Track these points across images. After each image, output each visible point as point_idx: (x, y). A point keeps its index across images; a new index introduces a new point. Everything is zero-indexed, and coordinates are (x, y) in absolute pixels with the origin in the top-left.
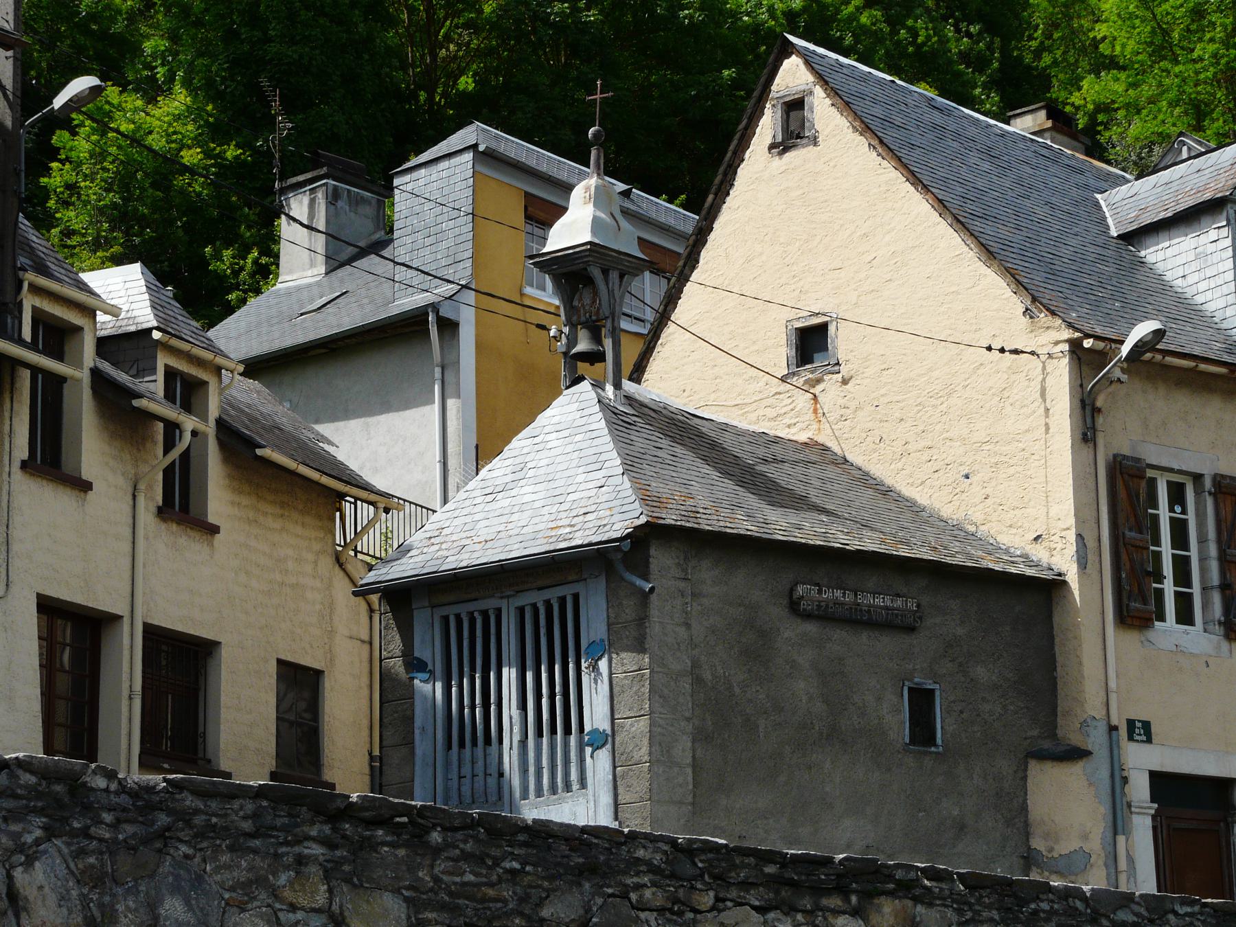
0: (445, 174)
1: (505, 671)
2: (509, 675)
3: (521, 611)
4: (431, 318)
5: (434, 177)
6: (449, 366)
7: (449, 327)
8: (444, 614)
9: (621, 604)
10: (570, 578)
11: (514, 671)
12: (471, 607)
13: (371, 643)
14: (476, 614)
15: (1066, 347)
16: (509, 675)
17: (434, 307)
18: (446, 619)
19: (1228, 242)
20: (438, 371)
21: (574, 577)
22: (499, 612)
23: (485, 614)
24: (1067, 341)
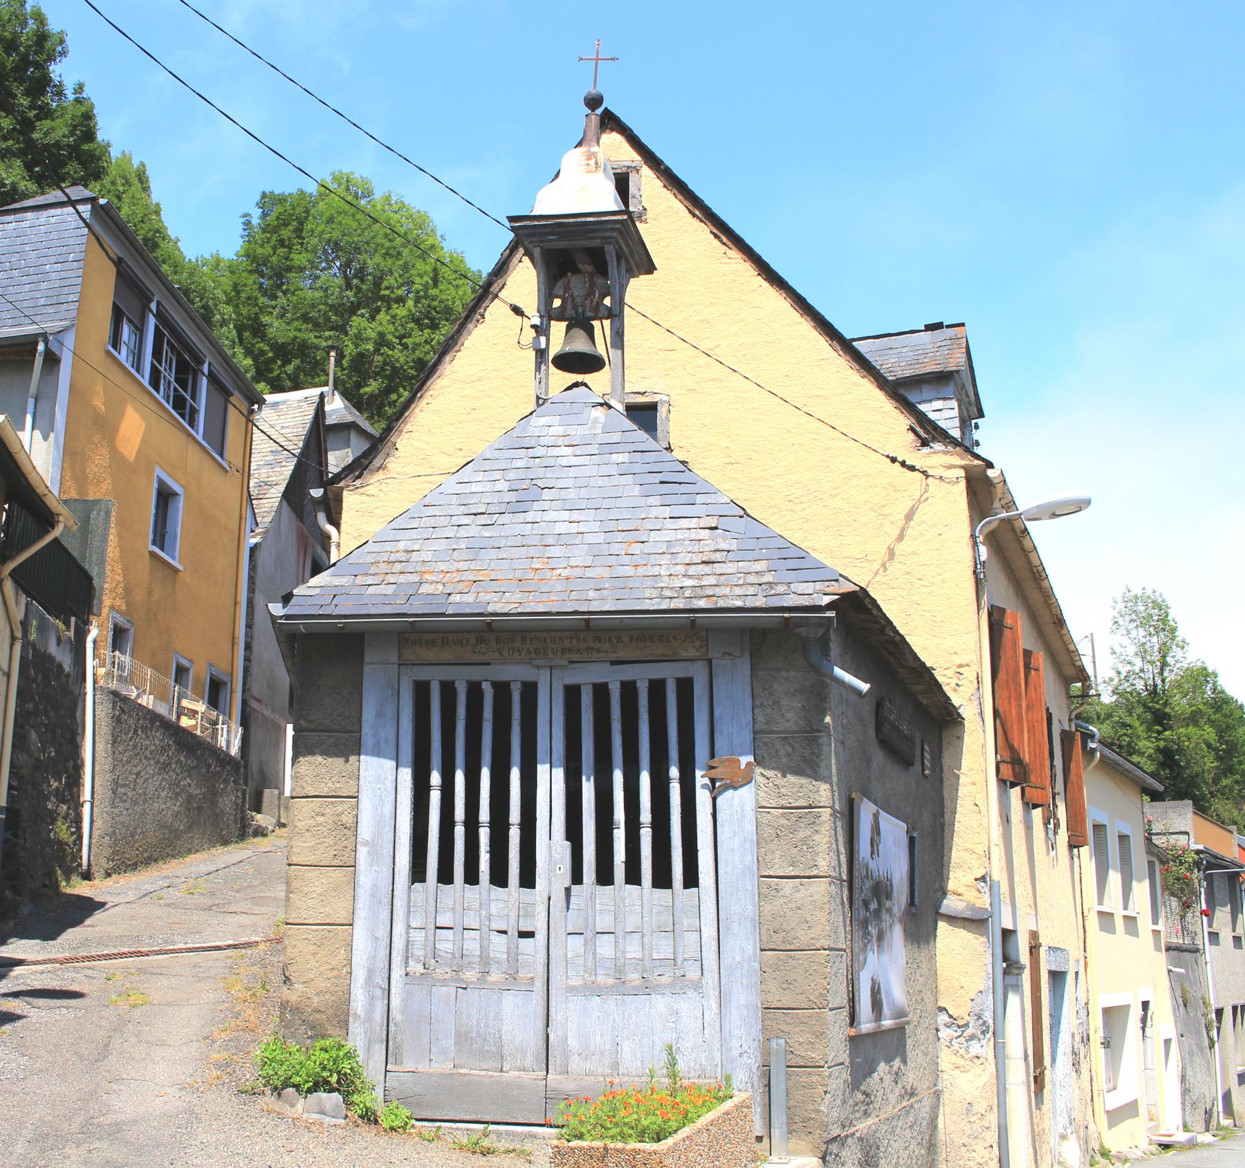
0: (53, 220)
1: (542, 770)
2: (551, 781)
3: (572, 694)
4: (41, 347)
5: (42, 220)
6: (45, 397)
7: (52, 360)
8: (422, 677)
9: (776, 703)
10: (684, 654)
11: (559, 774)
12: (475, 673)
13: (8, 675)
14: (486, 687)
15: (962, 473)
16: (551, 781)
17: (44, 336)
18: (422, 690)
19: (955, 413)
20: (31, 402)
21: (691, 653)
22: (530, 691)
23: (497, 685)
24: (962, 467)
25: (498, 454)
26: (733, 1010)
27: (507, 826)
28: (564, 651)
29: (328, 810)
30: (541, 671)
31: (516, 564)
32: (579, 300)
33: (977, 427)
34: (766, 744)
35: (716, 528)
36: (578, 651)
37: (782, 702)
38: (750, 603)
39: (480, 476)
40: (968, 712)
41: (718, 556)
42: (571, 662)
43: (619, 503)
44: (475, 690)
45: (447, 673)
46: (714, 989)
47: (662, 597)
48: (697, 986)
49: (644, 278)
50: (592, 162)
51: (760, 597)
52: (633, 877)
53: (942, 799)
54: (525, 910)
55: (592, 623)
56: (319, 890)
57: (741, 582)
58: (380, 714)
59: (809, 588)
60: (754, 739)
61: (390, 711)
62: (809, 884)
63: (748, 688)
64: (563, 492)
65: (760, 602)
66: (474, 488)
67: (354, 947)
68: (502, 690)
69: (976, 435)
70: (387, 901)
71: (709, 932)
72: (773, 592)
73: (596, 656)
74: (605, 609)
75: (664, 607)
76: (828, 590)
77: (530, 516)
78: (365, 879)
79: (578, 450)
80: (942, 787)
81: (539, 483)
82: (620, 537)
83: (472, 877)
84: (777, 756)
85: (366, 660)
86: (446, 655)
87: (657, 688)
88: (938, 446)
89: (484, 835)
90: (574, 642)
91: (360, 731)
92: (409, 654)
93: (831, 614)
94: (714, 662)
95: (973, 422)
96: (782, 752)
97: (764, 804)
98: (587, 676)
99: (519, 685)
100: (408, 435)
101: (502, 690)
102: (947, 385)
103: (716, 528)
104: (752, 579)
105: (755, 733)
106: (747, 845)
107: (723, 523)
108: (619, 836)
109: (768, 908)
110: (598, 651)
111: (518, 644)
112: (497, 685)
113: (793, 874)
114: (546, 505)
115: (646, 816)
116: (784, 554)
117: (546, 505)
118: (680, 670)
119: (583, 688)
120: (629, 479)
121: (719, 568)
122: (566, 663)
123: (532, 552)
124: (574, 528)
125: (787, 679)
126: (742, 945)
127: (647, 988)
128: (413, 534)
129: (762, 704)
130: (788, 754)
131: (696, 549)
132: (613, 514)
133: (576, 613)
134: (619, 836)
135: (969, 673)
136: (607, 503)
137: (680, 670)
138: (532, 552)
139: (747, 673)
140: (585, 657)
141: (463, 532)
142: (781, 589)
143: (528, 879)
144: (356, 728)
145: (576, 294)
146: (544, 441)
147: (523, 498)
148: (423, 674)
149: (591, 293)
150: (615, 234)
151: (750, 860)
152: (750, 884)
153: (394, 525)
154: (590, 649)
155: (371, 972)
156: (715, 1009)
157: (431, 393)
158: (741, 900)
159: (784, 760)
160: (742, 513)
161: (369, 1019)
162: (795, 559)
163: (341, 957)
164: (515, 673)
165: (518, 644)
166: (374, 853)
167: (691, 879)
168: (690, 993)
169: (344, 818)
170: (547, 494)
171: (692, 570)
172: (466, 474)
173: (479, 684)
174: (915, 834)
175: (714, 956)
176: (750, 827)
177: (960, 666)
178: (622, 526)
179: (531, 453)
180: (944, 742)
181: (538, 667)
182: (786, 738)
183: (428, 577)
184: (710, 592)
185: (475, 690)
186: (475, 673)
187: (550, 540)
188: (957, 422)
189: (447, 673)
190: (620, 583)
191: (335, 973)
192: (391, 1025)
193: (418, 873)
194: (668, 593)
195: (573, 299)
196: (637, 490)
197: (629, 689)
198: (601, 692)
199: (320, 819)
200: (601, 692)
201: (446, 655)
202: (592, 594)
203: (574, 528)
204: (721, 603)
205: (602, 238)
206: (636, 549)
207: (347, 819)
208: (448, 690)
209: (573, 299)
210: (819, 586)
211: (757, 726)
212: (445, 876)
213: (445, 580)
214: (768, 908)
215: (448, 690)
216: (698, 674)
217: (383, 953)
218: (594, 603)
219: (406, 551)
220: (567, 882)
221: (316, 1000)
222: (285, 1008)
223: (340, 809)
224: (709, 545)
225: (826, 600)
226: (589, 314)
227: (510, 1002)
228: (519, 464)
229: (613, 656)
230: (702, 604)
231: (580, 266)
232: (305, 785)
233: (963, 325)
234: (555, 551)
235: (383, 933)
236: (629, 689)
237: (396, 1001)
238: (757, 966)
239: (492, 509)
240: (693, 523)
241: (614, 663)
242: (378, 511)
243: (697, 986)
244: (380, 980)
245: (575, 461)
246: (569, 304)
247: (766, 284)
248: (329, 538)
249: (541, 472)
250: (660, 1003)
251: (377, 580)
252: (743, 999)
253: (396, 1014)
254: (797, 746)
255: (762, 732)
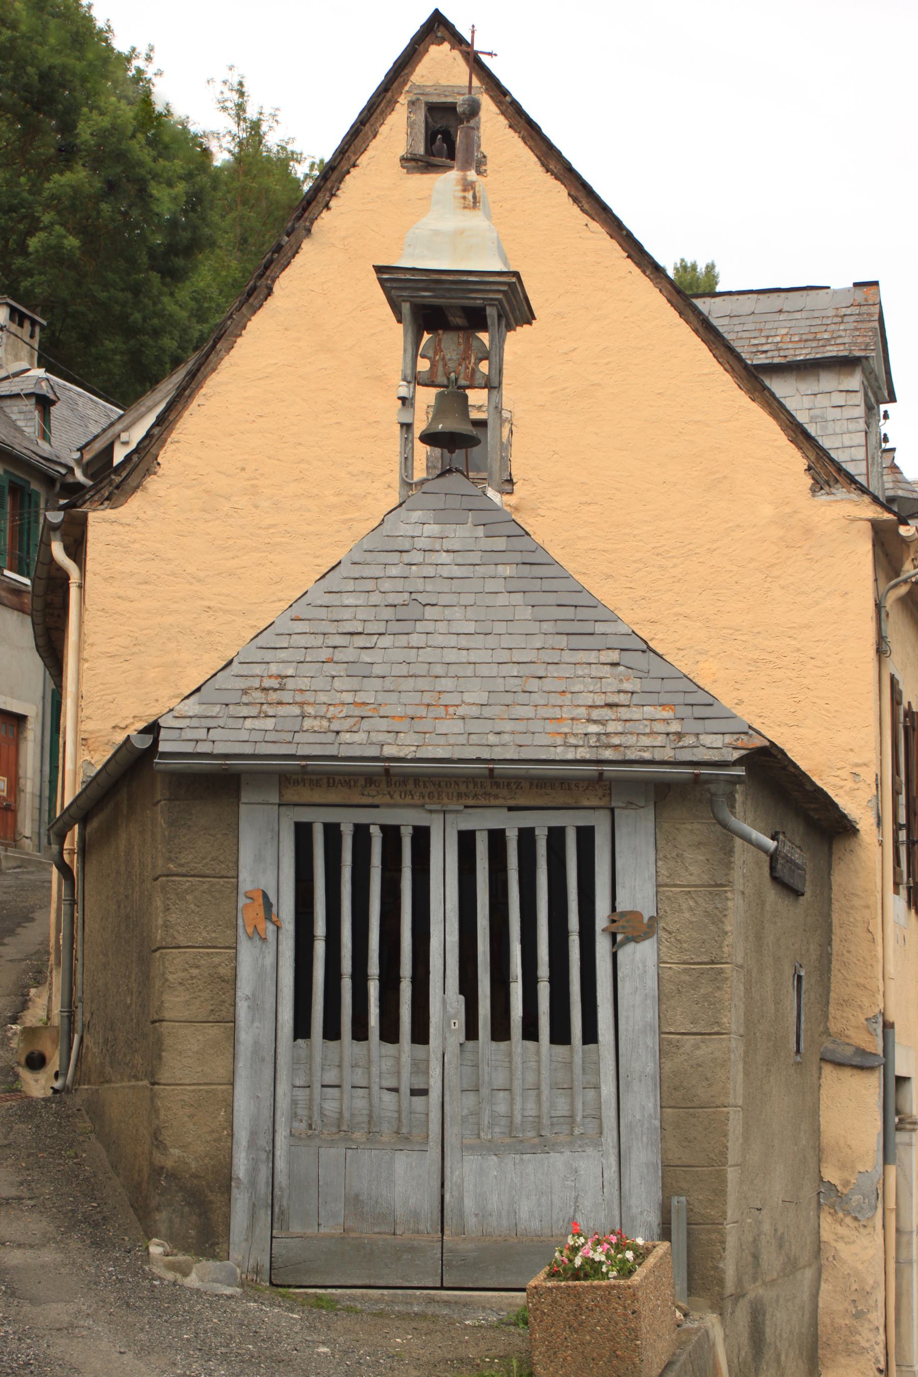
3: (466, 841)
10: (586, 803)
12: (362, 816)
14: (375, 831)
18: (303, 833)
21: (595, 802)
22: (422, 836)
24: (869, 520)
25: (369, 557)
26: (633, 1168)
27: (397, 980)
28: (460, 796)
29: (203, 962)
30: (434, 816)
31: (405, 698)
32: (451, 365)
33: (886, 416)
34: (668, 898)
35: (618, 664)
36: (475, 796)
37: (686, 854)
38: (659, 755)
39: (350, 585)
40: (865, 821)
41: (623, 699)
42: (466, 807)
43: (512, 627)
44: (361, 833)
45: (332, 816)
46: (613, 1147)
47: (566, 745)
48: (597, 1144)
49: (523, 331)
50: (469, 195)
51: (668, 749)
52: (530, 1032)
53: (830, 924)
54: (421, 1067)
55: (496, 772)
56: (195, 1048)
57: (648, 731)
58: (259, 858)
59: (718, 741)
60: (657, 892)
61: (270, 855)
62: (710, 1040)
63: (652, 840)
64: (447, 611)
65: (667, 754)
66: (349, 600)
67: (236, 1108)
68: (391, 834)
69: (885, 427)
70: (270, 1059)
71: (608, 1089)
72: (681, 744)
73: (493, 802)
74: (508, 757)
75: (570, 756)
76: (739, 743)
77: (415, 640)
78: (245, 1037)
79: (460, 559)
80: (830, 909)
81: (421, 598)
82: (515, 670)
83: (360, 1032)
84: (681, 911)
85: (243, 800)
86: (332, 797)
87: (556, 836)
88: (841, 493)
89: (374, 988)
90: (471, 786)
91: (237, 877)
92: (291, 795)
93: (740, 771)
94: (617, 812)
95: (883, 407)
96: (684, 906)
97: (666, 959)
98: (482, 822)
99: (410, 830)
100: (173, 447)
101: (391, 834)
102: (852, 373)
103: (618, 664)
104: (660, 727)
105: (658, 886)
106: (649, 1002)
107: (628, 658)
108: (517, 990)
109: (668, 1065)
110: (496, 797)
111: (411, 786)
112: (383, 828)
113: (694, 1030)
114: (430, 626)
115: (543, 971)
116: (690, 699)
117: (430, 626)
118: (583, 819)
119: (478, 834)
120: (518, 598)
121: (624, 713)
122: (462, 808)
123: (422, 684)
124: (463, 656)
125: (691, 831)
126: (642, 1103)
127: (545, 1146)
128: (282, 655)
129: (665, 857)
130: (691, 909)
131: (597, 688)
132: (506, 642)
133: (479, 760)
134: (517, 990)
135: (869, 775)
136: (500, 627)
137: (583, 819)
138: (422, 684)
139: (651, 825)
140: (483, 802)
141: (339, 655)
142: (689, 740)
143: (421, 1035)
144: (233, 873)
145: (448, 357)
146: (421, 543)
147: (406, 614)
148: (305, 815)
149: (465, 358)
150: (500, 296)
151: (651, 1015)
152: (651, 1041)
153: (260, 641)
154: (487, 795)
155: (253, 1135)
156: (614, 1168)
157: (203, 391)
158: (642, 1058)
159: (687, 915)
160: (645, 647)
161: (253, 1183)
162: (701, 705)
163: (220, 1118)
164: (407, 819)
165: (411, 786)
166: (255, 1007)
167: (590, 1035)
168: (590, 1150)
169: (222, 971)
170: (430, 612)
171: (595, 714)
172: (333, 581)
173: (367, 827)
174: (802, 974)
175: (613, 1113)
176: (652, 983)
177: (857, 765)
178: (517, 656)
179: (406, 558)
180: (835, 857)
181: (431, 811)
182: (689, 892)
183: (310, 710)
184: (616, 740)
185: (361, 833)
186: (362, 816)
187: (439, 670)
188: (860, 453)
189: (332, 816)
190: (520, 726)
191: (215, 1135)
192: (276, 1190)
193: (302, 1029)
194: (572, 740)
195: (445, 365)
196: (528, 613)
197: (527, 837)
198: (497, 838)
199: (195, 972)
200: (497, 838)
201: (332, 797)
202: (492, 739)
203: (463, 656)
204: (632, 755)
205: (483, 299)
206: (533, 685)
207: (224, 971)
208: (332, 832)
209: (445, 365)
210: (728, 739)
211: (660, 879)
212: (332, 1032)
213: (329, 715)
214: (668, 1065)
215: (332, 832)
216: (600, 824)
217: (267, 1113)
218: (496, 749)
219: (279, 676)
220: (462, 1038)
221: (193, 1165)
222: (160, 1175)
223: (216, 960)
224: (611, 684)
225: (736, 755)
226: (462, 382)
227: (403, 1163)
228: (394, 571)
229: (512, 803)
230: (608, 754)
231: (451, 318)
232: (175, 934)
233: (876, 284)
234: (446, 684)
235: (267, 1094)
236: (527, 837)
237: (280, 1164)
238: (657, 1123)
239: (371, 628)
240: (592, 657)
241: (510, 809)
242: (136, 546)
243: (597, 1144)
244: (263, 1141)
245: (457, 571)
246: (440, 368)
247: (637, 271)
248: (67, 578)
249: (420, 585)
250: (558, 1160)
251: (254, 711)
252: (643, 1157)
253: (282, 1179)
254: (700, 900)
255: (666, 885)
